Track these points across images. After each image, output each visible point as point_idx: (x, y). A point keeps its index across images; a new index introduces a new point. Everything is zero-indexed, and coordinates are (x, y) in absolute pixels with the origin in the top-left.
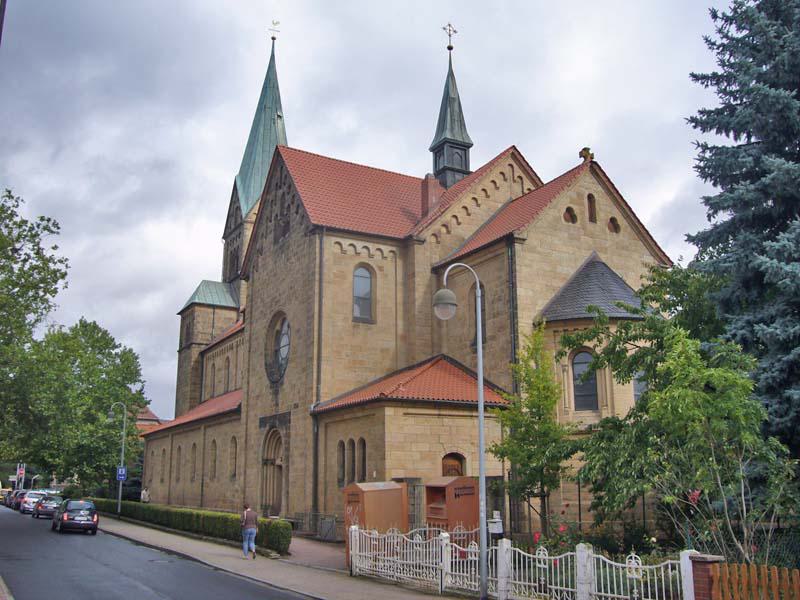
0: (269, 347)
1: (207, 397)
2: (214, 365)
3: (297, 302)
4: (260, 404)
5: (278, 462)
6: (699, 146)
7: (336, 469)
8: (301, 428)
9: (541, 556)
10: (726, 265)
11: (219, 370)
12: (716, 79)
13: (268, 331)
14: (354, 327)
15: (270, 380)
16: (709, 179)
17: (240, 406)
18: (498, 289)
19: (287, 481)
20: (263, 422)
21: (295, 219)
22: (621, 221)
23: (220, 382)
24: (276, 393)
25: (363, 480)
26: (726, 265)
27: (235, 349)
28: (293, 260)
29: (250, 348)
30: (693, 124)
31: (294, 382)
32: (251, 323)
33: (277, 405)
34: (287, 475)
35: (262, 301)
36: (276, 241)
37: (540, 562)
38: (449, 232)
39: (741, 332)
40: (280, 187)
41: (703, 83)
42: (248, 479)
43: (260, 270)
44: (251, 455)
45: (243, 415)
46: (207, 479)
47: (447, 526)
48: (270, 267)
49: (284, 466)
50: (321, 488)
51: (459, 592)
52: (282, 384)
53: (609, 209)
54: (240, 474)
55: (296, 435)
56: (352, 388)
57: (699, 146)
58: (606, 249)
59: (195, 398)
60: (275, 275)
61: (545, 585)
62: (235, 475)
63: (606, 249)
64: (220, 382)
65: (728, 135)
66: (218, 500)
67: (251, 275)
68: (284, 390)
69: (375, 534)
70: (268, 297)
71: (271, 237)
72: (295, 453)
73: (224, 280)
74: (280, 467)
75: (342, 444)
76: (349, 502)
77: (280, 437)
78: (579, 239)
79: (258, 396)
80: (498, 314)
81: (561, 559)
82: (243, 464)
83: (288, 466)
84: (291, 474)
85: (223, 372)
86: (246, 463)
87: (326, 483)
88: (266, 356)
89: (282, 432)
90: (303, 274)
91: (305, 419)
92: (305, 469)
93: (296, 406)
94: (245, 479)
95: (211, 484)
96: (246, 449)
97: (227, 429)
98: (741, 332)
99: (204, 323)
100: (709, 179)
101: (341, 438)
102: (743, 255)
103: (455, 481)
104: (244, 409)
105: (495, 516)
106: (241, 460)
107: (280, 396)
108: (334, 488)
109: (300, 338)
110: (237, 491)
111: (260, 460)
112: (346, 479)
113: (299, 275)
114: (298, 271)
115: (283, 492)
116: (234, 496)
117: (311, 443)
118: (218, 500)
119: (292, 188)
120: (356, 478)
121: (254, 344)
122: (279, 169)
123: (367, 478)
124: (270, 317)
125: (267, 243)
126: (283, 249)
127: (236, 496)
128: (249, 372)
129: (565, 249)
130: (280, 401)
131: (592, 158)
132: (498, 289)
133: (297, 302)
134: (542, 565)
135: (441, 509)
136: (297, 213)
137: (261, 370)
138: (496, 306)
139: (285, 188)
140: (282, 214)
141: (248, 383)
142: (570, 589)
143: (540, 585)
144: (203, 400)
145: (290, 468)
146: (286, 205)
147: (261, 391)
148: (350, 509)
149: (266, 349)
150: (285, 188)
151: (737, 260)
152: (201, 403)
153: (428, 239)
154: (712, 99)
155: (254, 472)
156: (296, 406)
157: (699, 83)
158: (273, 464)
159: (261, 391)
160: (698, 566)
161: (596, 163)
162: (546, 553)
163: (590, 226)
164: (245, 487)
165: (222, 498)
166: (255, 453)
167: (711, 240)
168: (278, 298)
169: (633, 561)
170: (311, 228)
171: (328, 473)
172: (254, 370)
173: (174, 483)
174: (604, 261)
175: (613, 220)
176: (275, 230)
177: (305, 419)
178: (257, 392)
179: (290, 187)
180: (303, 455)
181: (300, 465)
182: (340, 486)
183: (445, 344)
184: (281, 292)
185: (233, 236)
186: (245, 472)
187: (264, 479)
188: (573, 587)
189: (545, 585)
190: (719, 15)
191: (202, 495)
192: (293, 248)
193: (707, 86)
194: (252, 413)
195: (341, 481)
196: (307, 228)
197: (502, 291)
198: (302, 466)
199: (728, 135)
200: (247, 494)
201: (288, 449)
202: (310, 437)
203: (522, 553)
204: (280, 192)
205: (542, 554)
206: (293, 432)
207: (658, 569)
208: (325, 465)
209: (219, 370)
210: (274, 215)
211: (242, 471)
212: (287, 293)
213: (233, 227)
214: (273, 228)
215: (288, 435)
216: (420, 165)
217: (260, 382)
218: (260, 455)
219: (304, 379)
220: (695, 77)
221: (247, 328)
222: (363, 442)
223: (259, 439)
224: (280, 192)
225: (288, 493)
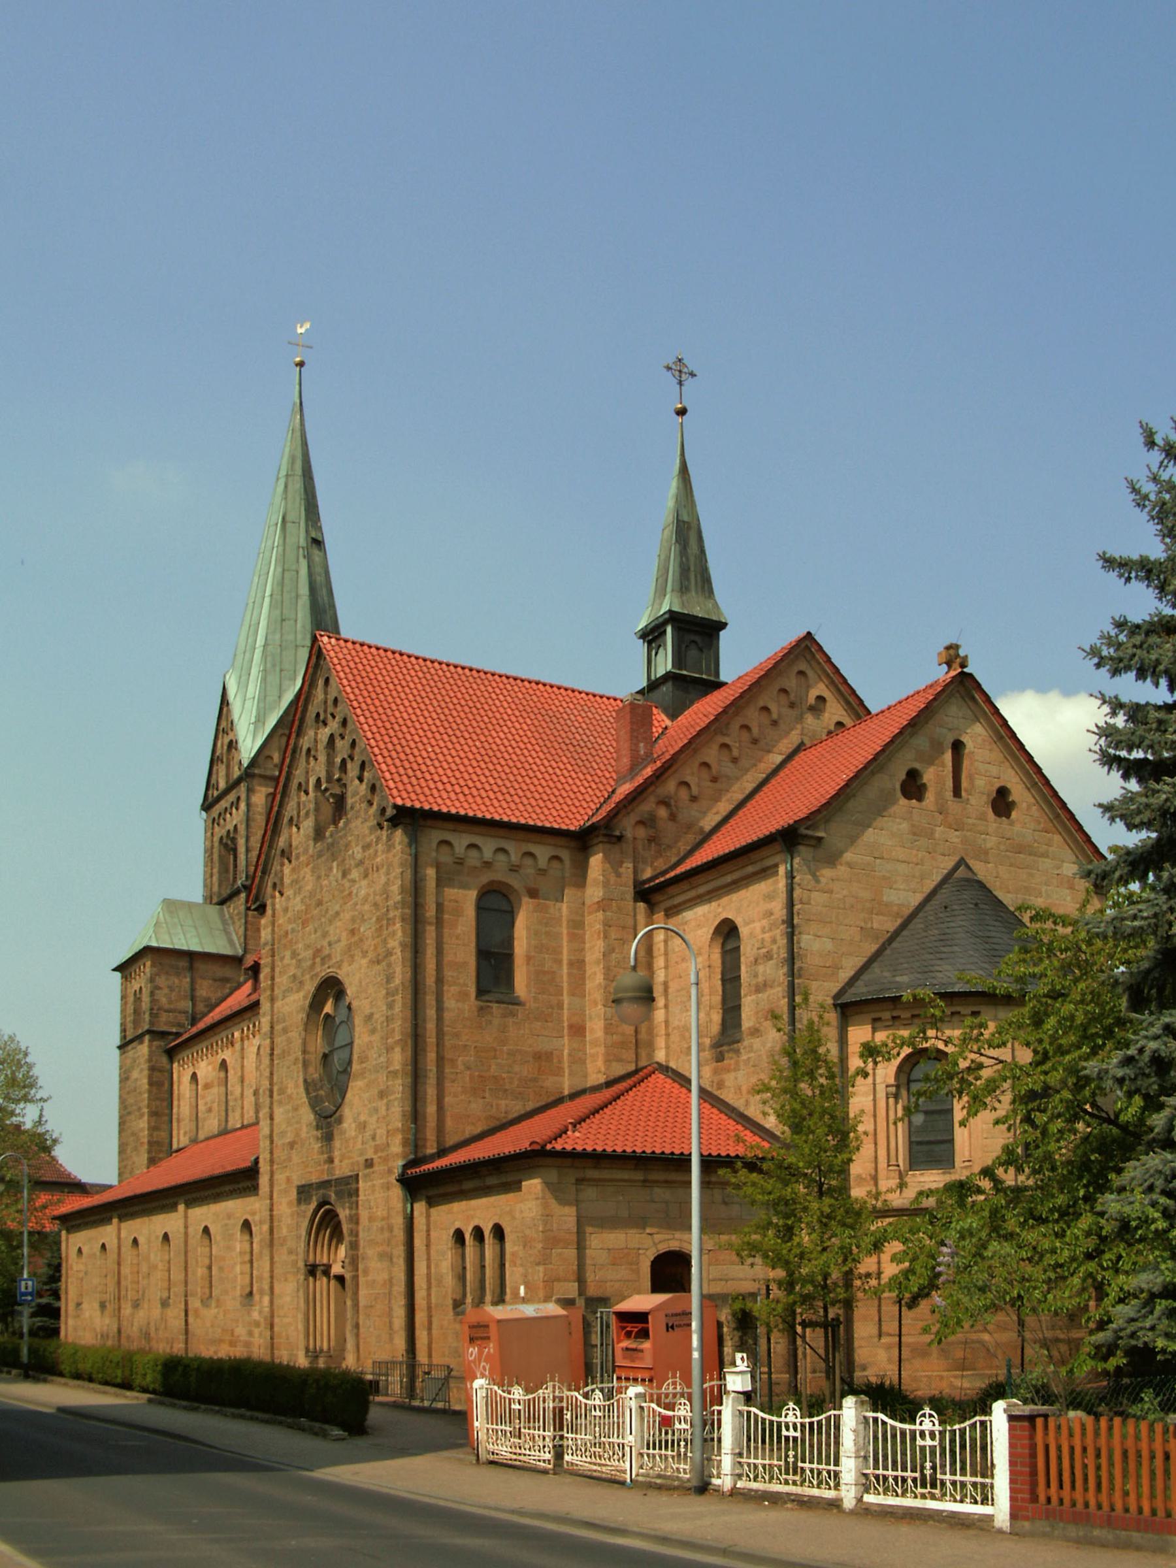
0: (311, 1049)
1: (184, 1141)
2: (194, 1076)
3: (364, 962)
4: (296, 1159)
5: (336, 1269)
6: (1104, 702)
7: (449, 1281)
8: (380, 1199)
9: (791, 1419)
10: (1136, 923)
11: (207, 1086)
12: (1147, 570)
13: (308, 1016)
14: (481, 1009)
15: (316, 1113)
16: (1115, 766)
17: (257, 1161)
18: (767, 936)
19: (356, 1305)
20: (304, 1192)
21: (357, 791)
22: (1019, 793)
23: (210, 1110)
24: (328, 1138)
25: (500, 1300)
26: (1136, 923)
27: (238, 1046)
28: (355, 874)
29: (272, 1049)
30: (1096, 660)
31: (362, 1118)
32: (272, 1000)
33: (331, 1160)
34: (356, 1293)
35: (294, 954)
36: (319, 834)
37: (914, 1480)
38: (673, 817)
39: (1153, 1045)
40: (325, 724)
41: (1121, 576)
42: (277, 1302)
43: (289, 892)
44: (282, 1256)
45: (264, 1180)
46: (194, 1303)
47: (651, 1380)
48: (309, 887)
49: (348, 1276)
50: (420, 1317)
51: (659, 1481)
52: (340, 1121)
53: (994, 770)
54: (262, 1292)
55: (371, 1219)
56: (478, 1130)
57: (1104, 702)
58: (986, 853)
59: (158, 1143)
60: (320, 903)
61: (795, 1463)
62: (251, 1293)
63: (986, 853)
64: (210, 1110)
65: (1157, 685)
66: (221, 1341)
67: (269, 903)
68: (343, 1132)
69: (518, 1393)
70: (307, 947)
71: (308, 825)
72: (369, 1252)
73: (209, 899)
74: (341, 1279)
75: (459, 1236)
76: (472, 1340)
77: (339, 1224)
78: (931, 835)
79: (292, 1145)
80: (765, 985)
81: (819, 1422)
82: (267, 1275)
83: (356, 1278)
84: (362, 1292)
85: (215, 1090)
86: (272, 1271)
87: (429, 1308)
88: (305, 1065)
89: (343, 1214)
90: (376, 905)
91: (387, 1187)
92: (391, 1281)
93: (369, 1164)
94: (272, 1302)
95: (205, 1312)
96: (271, 1244)
97: (236, 1208)
98: (1153, 1045)
99: (171, 989)
100: (1115, 766)
101: (458, 1225)
102: (1165, 907)
103: (669, 1300)
104: (264, 1167)
105: (739, 1362)
106: (262, 1266)
107: (337, 1143)
108: (445, 1319)
109: (373, 1031)
110: (257, 1324)
111: (301, 1264)
112: (469, 1299)
113: (367, 907)
114: (365, 900)
115: (349, 1327)
116: (250, 1334)
117: (400, 1234)
118: (221, 1341)
119: (350, 726)
120: (488, 1298)
121: (280, 1040)
122: (321, 682)
123: (508, 1297)
124: (310, 987)
125: (299, 836)
126: (333, 852)
127: (256, 1331)
128: (271, 1096)
129: (900, 853)
130: (337, 1154)
131: (963, 666)
132: (767, 936)
133: (364, 962)
134: (792, 1433)
135: (642, 1351)
136: (361, 779)
137: (295, 1088)
138: (761, 969)
139: (333, 726)
140: (329, 779)
141: (272, 1119)
142: (832, 1467)
143: (787, 1463)
144: (175, 1147)
145: (362, 1280)
146: (338, 760)
147: (297, 1135)
148: (473, 1351)
149: (304, 1052)
150: (333, 726)
151: (1155, 915)
152: (171, 1152)
153: (629, 834)
154: (1143, 603)
155: (290, 1290)
156: (369, 1164)
157: (1113, 575)
158: (326, 1272)
159: (297, 1135)
160: (1018, 1424)
161: (970, 675)
162: (798, 1413)
163: (953, 805)
164: (272, 1316)
165: (228, 1338)
166: (290, 1252)
167: (1117, 874)
168: (326, 951)
169: (927, 1420)
170: (390, 812)
171: (434, 1291)
172: (282, 1091)
173: (127, 1310)
174: (980, 877)
175: (1002, 792)
176: (317, 810)
177: (387, 1187)
178: (289, 1138)
179: (344, 723)
180: (388, 1257)
181: (379, 1273)
182: (457, 1314)
183: (660, 1042)
184: (333, 938)
185: (224, 804)
186: (272, 1288)
187: (310, 1302)
188: (837, 1463)
189: (795, 1463)
190: (1158, 440)
191: (187, 1332)
192: (357, 852)
193: (1128, 579)
194: (280, 1177)
195: (458, 1304)
196: (383, 811)
197: (774, 941)
198: (386, 1276)
199: (1157, 685)
200: (276, 1329)
201: (354, 1246)
202: (399, 1221)
203: (761, 1414)
204: (324, 733)
205: (792, 1415)
206: (364, 1214)
207: (973, 1426)
208: (429, 1275)
209: (207, 1086)
210: (312, 781)
211: (266, 1287)
212: (343, 943)
213: (222, 785)
214: (312, 806)
215: (355, 1220)
216: (624, 671)
217: (295, 1117)
218: (301, 1256)
219: (383, 1111)
220: (1109, 562)
221: (265, 1006)
222: (499, 1232)
223: (298, 1226)
224: (324, 733)
225: (357, 1326)
